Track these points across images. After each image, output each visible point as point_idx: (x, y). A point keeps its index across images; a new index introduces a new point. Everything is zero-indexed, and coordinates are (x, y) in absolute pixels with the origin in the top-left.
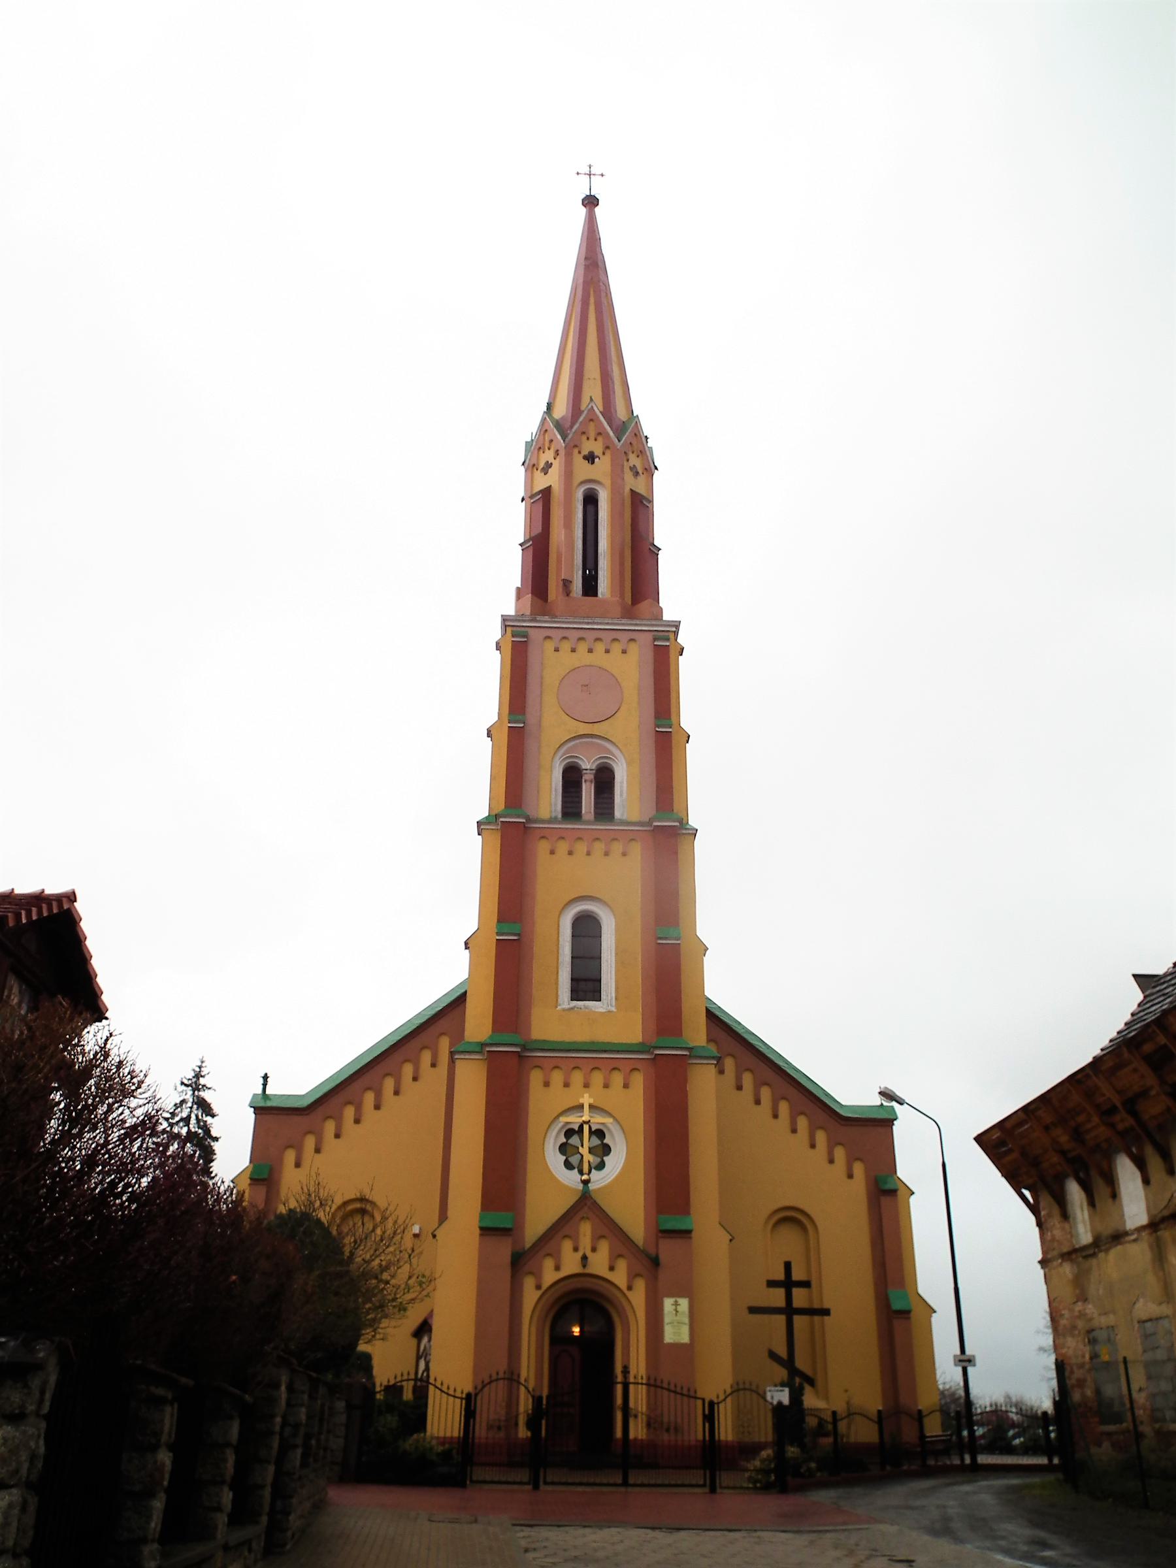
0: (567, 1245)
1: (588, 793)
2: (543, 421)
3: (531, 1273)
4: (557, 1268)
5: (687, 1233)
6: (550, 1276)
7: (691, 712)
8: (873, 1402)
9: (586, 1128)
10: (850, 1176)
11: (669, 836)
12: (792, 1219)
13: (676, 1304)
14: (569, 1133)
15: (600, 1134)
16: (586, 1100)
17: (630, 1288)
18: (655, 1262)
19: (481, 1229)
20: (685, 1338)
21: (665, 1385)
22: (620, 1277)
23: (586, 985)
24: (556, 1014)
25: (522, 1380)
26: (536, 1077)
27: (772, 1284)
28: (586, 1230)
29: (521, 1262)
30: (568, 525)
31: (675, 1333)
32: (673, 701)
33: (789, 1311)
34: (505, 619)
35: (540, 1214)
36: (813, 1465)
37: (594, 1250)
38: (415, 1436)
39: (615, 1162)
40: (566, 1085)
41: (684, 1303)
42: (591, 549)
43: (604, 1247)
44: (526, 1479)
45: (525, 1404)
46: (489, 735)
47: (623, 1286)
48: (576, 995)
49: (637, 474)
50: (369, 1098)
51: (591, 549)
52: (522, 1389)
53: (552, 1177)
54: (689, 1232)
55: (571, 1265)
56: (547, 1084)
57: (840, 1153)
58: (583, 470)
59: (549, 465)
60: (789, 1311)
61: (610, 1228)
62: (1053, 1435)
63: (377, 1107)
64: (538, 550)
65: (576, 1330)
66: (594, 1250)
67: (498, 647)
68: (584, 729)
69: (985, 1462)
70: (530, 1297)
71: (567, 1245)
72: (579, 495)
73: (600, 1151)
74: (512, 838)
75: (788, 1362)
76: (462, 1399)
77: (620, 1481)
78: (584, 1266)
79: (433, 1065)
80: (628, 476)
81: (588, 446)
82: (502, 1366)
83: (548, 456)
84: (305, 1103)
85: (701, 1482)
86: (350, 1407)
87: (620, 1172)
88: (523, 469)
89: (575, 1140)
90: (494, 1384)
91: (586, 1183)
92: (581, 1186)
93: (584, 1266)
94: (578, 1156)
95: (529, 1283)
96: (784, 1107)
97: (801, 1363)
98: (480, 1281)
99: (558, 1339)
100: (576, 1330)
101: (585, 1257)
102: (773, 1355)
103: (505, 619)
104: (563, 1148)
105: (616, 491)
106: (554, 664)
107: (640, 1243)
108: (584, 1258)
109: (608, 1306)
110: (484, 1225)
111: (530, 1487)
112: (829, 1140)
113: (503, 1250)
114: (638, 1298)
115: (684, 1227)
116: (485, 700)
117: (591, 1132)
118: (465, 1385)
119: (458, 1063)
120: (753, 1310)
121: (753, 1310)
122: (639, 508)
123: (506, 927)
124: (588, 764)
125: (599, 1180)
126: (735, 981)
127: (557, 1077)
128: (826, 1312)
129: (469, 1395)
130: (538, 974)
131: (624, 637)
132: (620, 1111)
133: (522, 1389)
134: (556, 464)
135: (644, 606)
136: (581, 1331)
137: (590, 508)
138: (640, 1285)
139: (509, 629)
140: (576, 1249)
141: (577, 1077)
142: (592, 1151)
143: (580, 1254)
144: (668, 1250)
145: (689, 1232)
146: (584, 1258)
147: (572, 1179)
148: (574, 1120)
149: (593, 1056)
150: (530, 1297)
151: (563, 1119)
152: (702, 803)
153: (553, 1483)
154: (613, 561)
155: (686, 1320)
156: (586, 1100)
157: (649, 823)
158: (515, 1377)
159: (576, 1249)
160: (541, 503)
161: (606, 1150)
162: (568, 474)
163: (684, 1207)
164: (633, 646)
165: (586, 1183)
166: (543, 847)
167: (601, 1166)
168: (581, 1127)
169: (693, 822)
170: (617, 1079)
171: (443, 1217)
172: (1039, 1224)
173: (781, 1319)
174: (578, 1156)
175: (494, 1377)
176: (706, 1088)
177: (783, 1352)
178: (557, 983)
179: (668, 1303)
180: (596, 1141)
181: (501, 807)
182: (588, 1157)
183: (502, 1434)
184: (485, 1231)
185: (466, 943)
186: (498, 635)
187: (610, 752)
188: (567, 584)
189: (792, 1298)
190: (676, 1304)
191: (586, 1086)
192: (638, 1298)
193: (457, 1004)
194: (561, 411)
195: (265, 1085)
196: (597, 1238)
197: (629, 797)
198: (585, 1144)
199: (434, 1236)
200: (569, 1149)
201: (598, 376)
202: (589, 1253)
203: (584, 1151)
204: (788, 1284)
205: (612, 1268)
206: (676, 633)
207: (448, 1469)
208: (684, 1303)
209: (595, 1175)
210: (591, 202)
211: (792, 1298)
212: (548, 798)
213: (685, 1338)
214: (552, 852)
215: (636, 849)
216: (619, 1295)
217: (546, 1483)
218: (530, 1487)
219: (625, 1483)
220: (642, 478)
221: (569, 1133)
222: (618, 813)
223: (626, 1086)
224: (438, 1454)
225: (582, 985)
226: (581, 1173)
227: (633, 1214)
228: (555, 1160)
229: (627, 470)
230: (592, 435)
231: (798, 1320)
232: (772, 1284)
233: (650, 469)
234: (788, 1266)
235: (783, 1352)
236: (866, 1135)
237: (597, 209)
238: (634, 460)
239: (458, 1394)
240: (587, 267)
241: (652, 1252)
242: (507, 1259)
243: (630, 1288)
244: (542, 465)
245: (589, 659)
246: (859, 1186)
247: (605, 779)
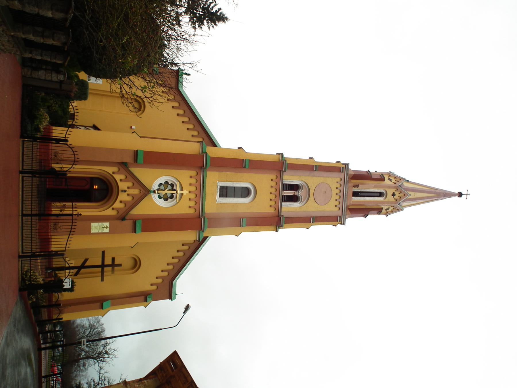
0: (130, 184)
1: (290, 193)
2: (404, 179)
3: (119, 170)
4: (121, 180)
5: (134, 231)
6: (118, 177)
7: (316, 229)
9: (175, 192)
10: (152, 285)
11: (276, 221)
12: (136, 264)
13: (107, 227)
14: (172, 185)
15: (172, 197)
16: (185, 192)
17: (113, 209)
18: (123, 219)
19: (137, 151)
20: (93, 231)
21: (74, 224)
22: (117, 205)
23: (225, 192)
24: (215, 180)
25: (74, 166)
26: (193, 173)
27: (113, 259)
28: (136, 192)
29: (124, 166)
30: (375, 187)
31: (95, 227)
32: (320, 223)
33: (103, 266)
34: (347, 165)
35: (142, 173)
36: (35, 300)
37: (128, 195)
38: (48, 117)
39: (161, 203)
40: (190, 185)
41: (107, 230)
42: (365, 194)
43: (129, 199)
44: (24, 168)
45: (66, 167)
46: (310, 158)
47: (114, 206)
48: (222, 188)
49: (386, 210)
50: (181, 112)
51: (365, 194)
52: (70, 166)
53: (156, 178)
54: (135, 232)
55: (123, 186)
56: (191, 177)
57: (160, 281)
58: (390, 192)
59: (391, 180)
60: (103, 266)
61: (137, 201)
62: (59, 343)
63: (178, 115)
64: (366, 176)
65: (96, 187)
66: (128, 195)
68: (312, 192)
69: (42, 354)
70: (110, 170)
71: (130, 184)
72: (382, 191)
73: (165, 197)
74: (279, 165)
75: (83, 266)
76: (65, 137)
77: (24, 213)
78: (122, 191)
79: (193, 136)
80: (386, 207)
81: (397, 193)
82: (81, 158)
83: (394, 181)
84: (180, 88)
85: (24, 251)
86: (61, 82)
87: (157, 205)
88: (388, 172)
89: (169, 187)
90: (72, 153)
91: (154, 192)
92: (152, 190)
93: (122, 191)
94: (163, 189)
95: (115, 169)
96: (176, 260)
97: (83, 270)
98: (116, 150)
99: (92, 180)
100: (96, 187)
101: (125, 191)
102: (86, 260)
103: (347, 165)
104: (166, 183)
105: (383, 203)
106: (333, 181)
107: (131, 213)
108: (125, 191)
109: (106, 200)
110: (138, 151)
111: (21, 169)
112: (164, 277)
113: (128, 159)
114: (109, 212)
115: (137, 228)
117: (172, 194)
118: (72, 141)
119: (199, 143)
120: (103, 253)
121: (103, 253)
122: (379, 211)
123: (247, 163)
125: (155, 197)
127: (193, 181)
128: (102, 280)
129: (67, 141)
130: (230, 174)
131: (341, 206)
132: (182, 206)
133: (70, 166)
134: (391, 183)
135: (349, 212)
136: (96, 189)
137: (378, 194)
138: (114, 213)
139: (344, 166)
140: (128, 188)
141: (193, 188)
142: (163, 193)
143: (127, 189)
144: (128, 224)
145: (135, 232)
146: (125, 191)
147: (155, 187)
148: (178, 188)
150: (110, 170)
151: (178, 183)
152: (287, 233)
153: (23, 180)
154: (363, 202)
155: (100, 232)
156: (185, 192)
157: (281, 215)
158: (76, 163)
159: (128, 188)
160: (381, 178)
161: (166, 199)
162: (389, 187)
163: (144, 230)
164: (337, 209)
165: (154, 192)
167: (160, 197)
168: (175, 190)
169: (281, 230)
170: (192, 204)
171: (141, 137)
172: (140, 380)
173: (100, 264)
174: (163, 189)
175: (76, 153)
176: (190, 236)
177: (87, 264)
178: (227, 181)
179: (107, 224)
180: (169, 195)
181: (288, 162)
182: (163, 193)
183: (53, 157)
184: (136, 152)
185: (241, 148)
186: (343, 162)
187: (304, 201)
188: (357, 186)
189: (106, 266)
190: (107, 227)
191: (190, 192)
192: (109, 212)
193: (214, 144)
194: (406, 185)
195: (186, 74)
196: (133, 197)
197: (289, 208)
198: (169, 191)
199: (133, 132)
200: (166, 185)
201: (415, 197)
202: (127, 193)
203: (166, 191)
204: (113, 265)
205: (121, 202)
206: (341, 224)
207: (29, 128)
208: (107, 230)
209: (156, 195)
210: (460, 195)
211: (106, 266)
212: (289, 179)
213: (93, 231)
214: (272, 180)
215: (272, 210)
216: (110, 204)
217: (23, 177)
218: (21, 169)
219: (23, 215)
221: (172, 185)
222: (283, 203)
223: (190, 207)
224: (38, 125)
225: (225, 191)
226: (158, 190)
227: (142, 210)
228: (162, 180)
229: (389, 207)
230: (400, 195)
231: (100, 269)
232: (113, 259)
233: (387, 214)
234: (120, 265)
235: (87, 264)
236: (167, 291)
237: (457, 197)
238: (391, 209)
239: (67, 136)
240: (444, 193)
241: (127, 217)
242: (125, 161)
243: (113, 209)
244: (391, 178)
245: (334, 194)
246: (148, 288)
247: (294, 199)
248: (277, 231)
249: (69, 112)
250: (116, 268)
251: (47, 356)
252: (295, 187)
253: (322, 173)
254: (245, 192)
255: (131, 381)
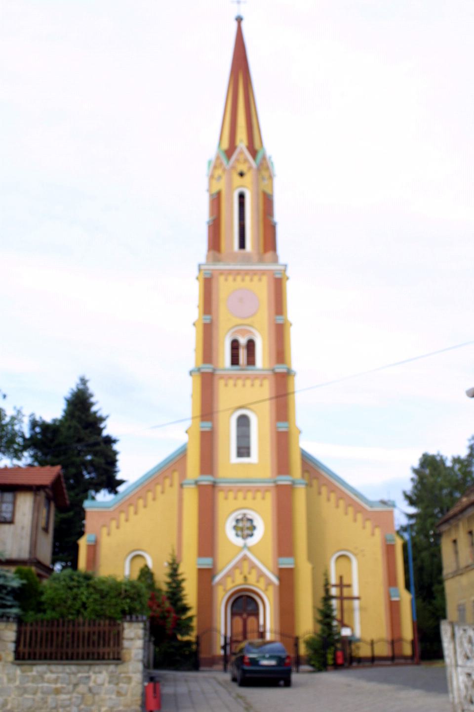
1: (243, 354)
4: (233, 581)
8: (292, 655)
11: (282, 385)
23: (243, 450)
37: (250, 573)
39: (259, 534)
55: (239, 580)
67: (197, 278)
68: (240, 321)
74: (207, 383)
105: (256, 195)
106: (225, 288)
116: (192, 311)
122: (267, 203)
124: (243, 341)
126: (310, 442)
140: (241, 573)
146: (245, 578)
149: (246, 487)
160: (216, 201)
166: (221, 383)
193: (181, 455)
198: (245, 528)
210: (239, 20)
220: (266, 182)
233: (271, 177)
234: (341, 578)
247: (251, 345)
248: (270, 157)
249: (92, 489)
250: (345, 582)
251: (411, 564)
252: (235, 345)
253: (214, 303)
254: (243, 422)
255: (439, 551)
